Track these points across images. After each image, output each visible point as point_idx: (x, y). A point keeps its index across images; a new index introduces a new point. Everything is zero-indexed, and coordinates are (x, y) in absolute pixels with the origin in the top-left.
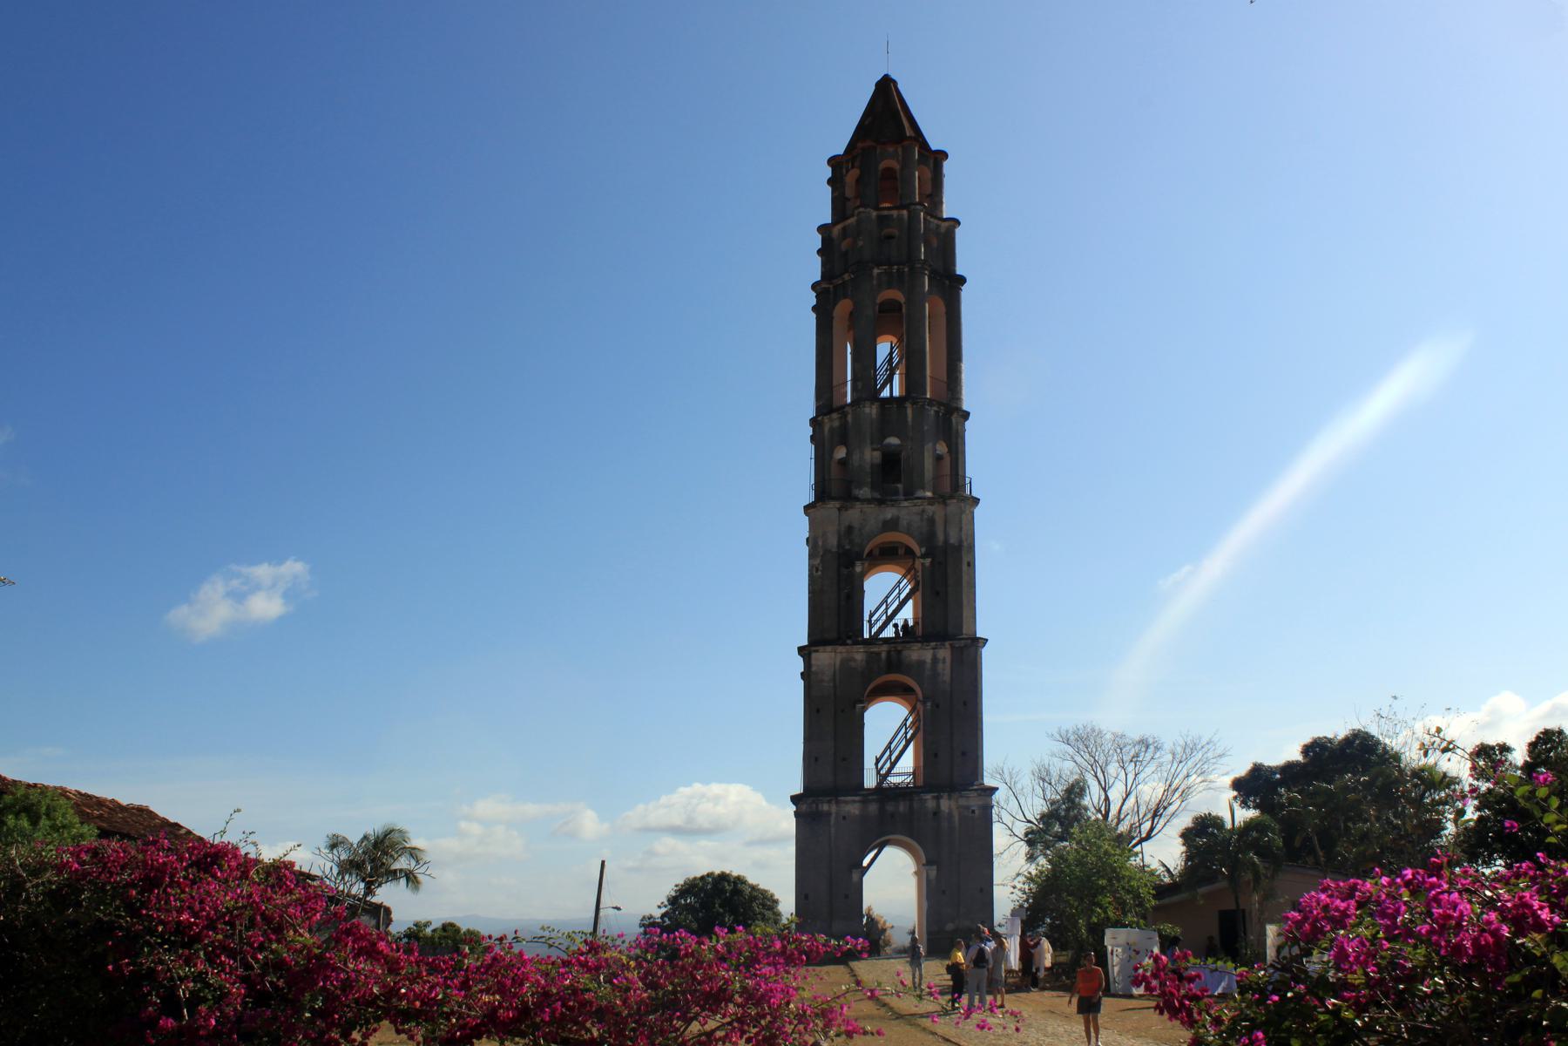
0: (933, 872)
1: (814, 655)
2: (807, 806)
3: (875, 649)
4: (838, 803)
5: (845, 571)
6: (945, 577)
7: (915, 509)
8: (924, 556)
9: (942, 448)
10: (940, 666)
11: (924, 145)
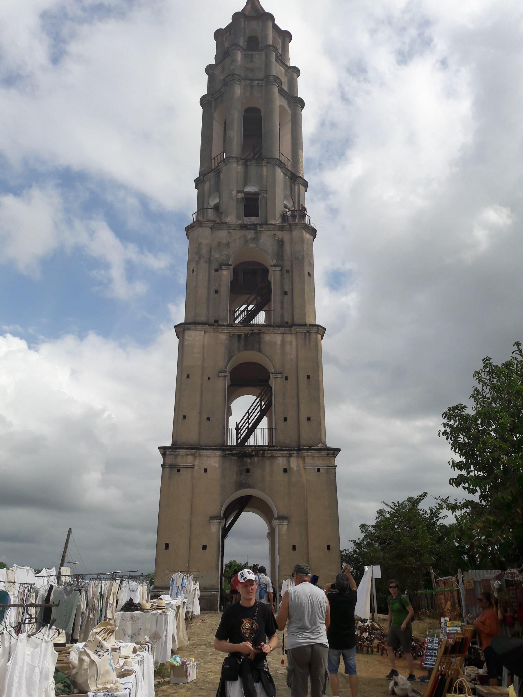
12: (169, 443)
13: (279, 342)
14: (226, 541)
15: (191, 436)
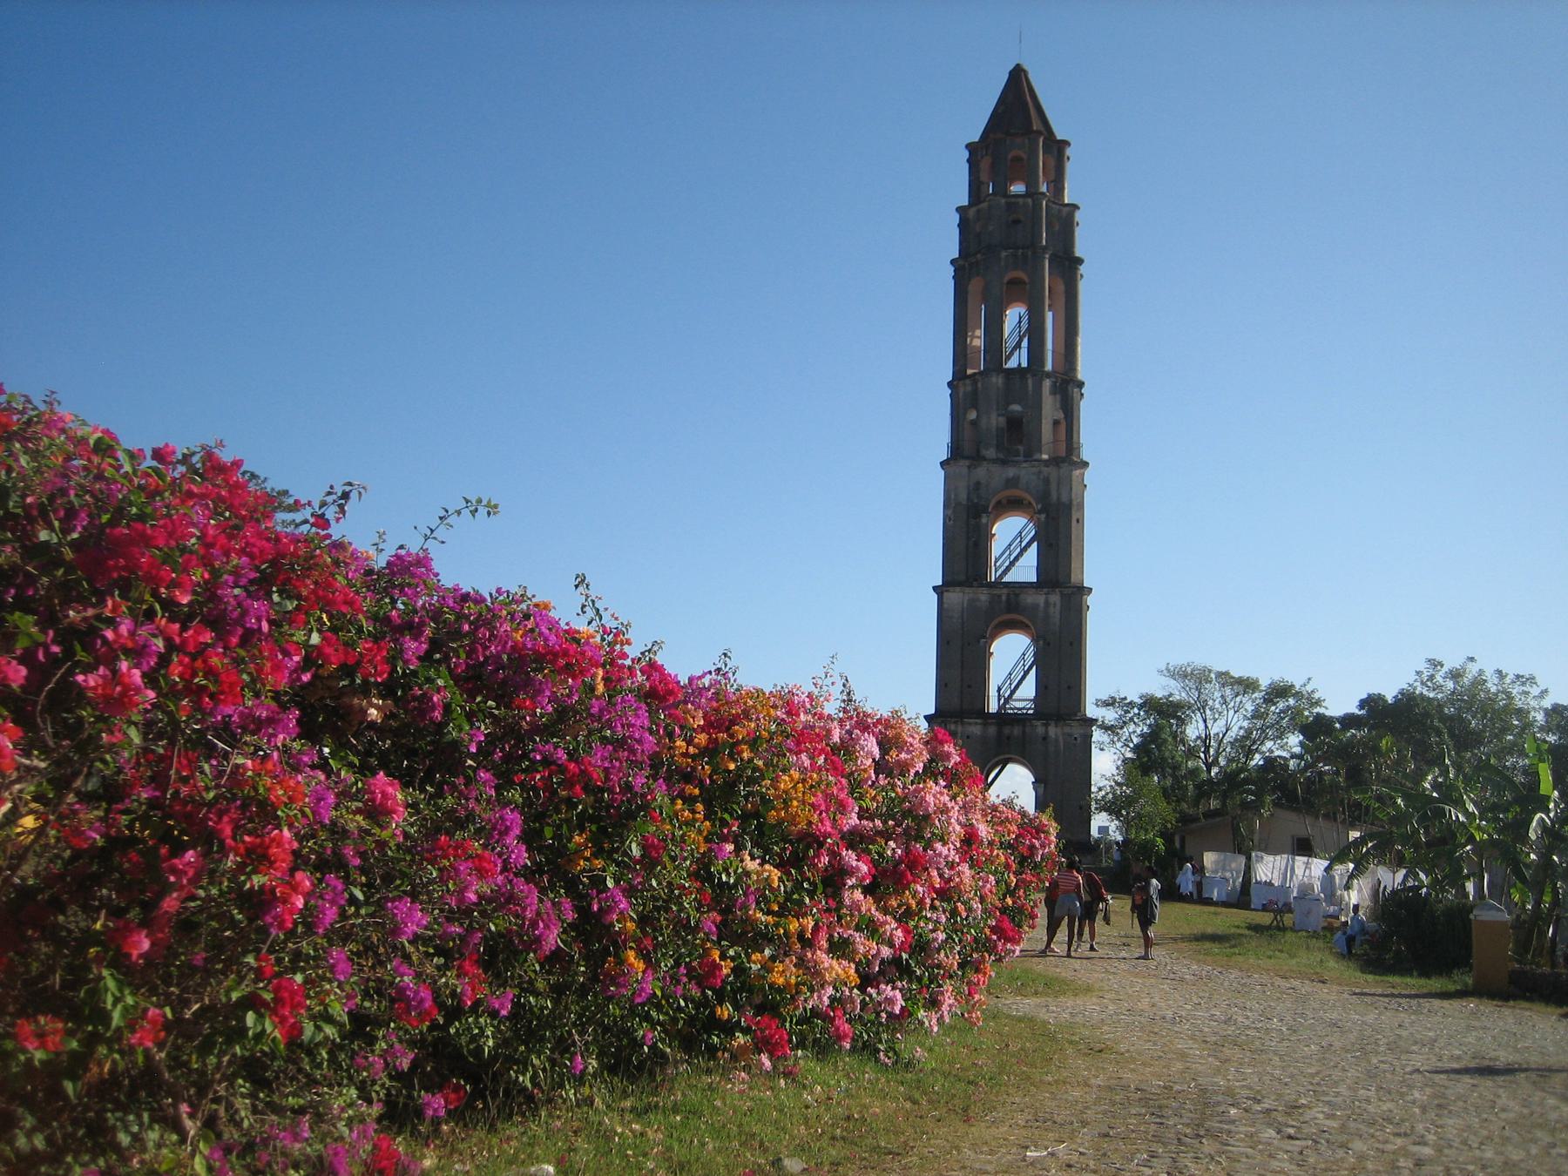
0: (1041, 790)
3: (997, 592)
5: (972, 521)
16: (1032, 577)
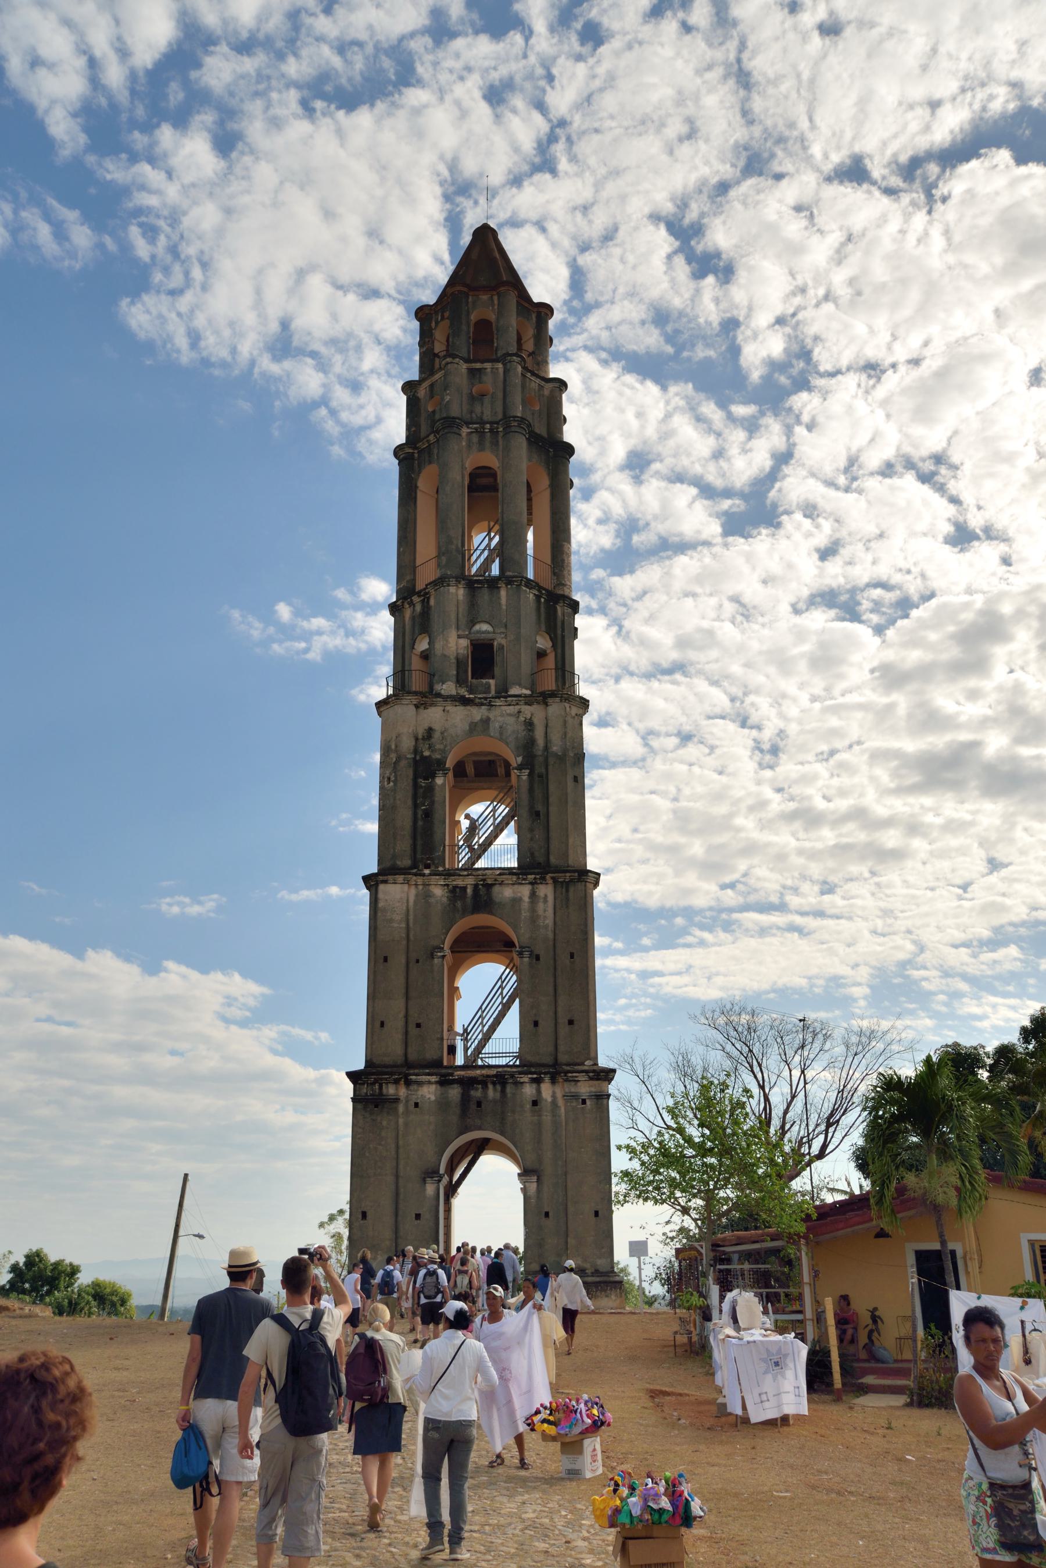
0: (533, 1187)
1: (382, 887)
2: (371, 1089)
3: (459, 882)
4: (408, 1083)
5: (422, 783)
6: (547, 783)
7: (511, 709)
8: (520, 768)
9: (543, 642)
10: (541, 906)
11: (523, 294)
12: (374, 869)
13: (526, 899)
14: (457, 1202)
15: (393, 1050)
16: (511, 862)
